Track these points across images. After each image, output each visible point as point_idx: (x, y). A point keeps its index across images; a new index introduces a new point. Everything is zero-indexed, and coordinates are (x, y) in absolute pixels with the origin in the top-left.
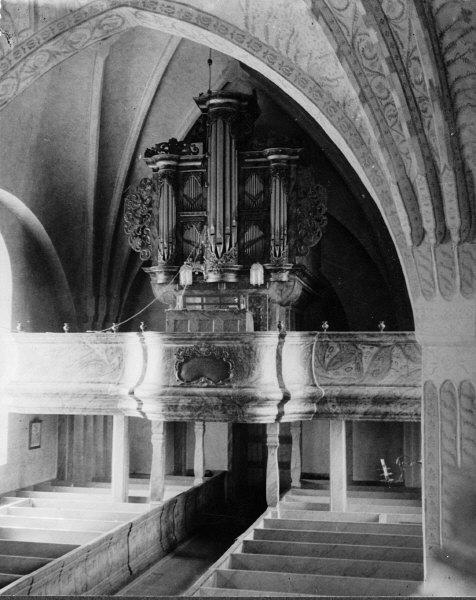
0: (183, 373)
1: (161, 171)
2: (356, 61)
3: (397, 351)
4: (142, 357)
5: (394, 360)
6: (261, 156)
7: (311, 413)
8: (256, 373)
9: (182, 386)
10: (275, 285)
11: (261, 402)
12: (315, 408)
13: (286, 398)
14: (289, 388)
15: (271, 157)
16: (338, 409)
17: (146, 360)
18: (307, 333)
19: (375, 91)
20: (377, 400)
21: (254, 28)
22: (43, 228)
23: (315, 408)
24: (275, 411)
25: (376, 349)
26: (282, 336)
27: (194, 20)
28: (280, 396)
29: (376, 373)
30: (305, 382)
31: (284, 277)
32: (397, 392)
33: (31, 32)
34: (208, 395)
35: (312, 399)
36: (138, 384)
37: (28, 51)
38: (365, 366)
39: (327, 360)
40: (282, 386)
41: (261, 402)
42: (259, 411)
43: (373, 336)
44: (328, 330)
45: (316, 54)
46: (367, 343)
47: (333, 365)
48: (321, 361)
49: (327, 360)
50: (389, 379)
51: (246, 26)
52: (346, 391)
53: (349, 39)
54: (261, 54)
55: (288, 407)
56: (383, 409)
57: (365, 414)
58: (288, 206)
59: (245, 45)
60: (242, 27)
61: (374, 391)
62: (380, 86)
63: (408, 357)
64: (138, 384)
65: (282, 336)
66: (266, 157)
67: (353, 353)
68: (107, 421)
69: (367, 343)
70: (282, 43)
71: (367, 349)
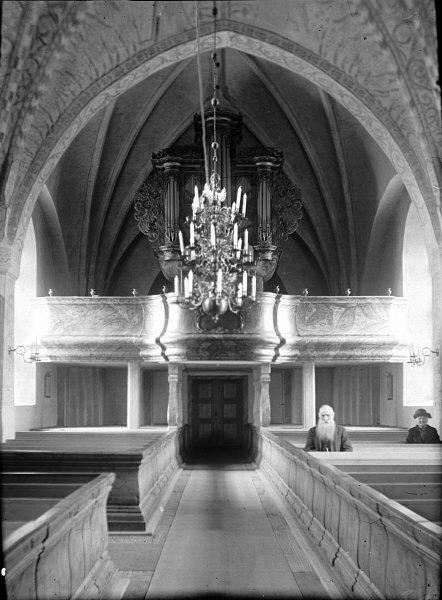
0: (203, 324)
1: (167, 170)
2: (410, 79)
3: (358, 310)
4: (163, 312)
5: (357, 317)
6: (251, 162)
7: (295, 356)
8: (261, 325)
9: (203, 333)
10: (261, 263)
11: (264, 344)
12: (297, 352)
13: (283, 342)
14: (283, 336)
15: (258, 164)
16: (315, 353)
17: (167, 316)
18: (293, 296)
19: (421, 99)
20: (345, 346)
21: (325, 54)
22: (56, 212)
23: (297, 352)
24: (273, 353)
25: (343, 309)
26: (278, 298)
27: (280, 44)
28: (278, 341)
29: (343, 327)
30: (292, 332)
31: (269, 256)
32: (361, 340)
33: (151, 43)
34: (225, 339)
35: (297, 346)
36: (162, 334)
37: (149, 56)
38: (335, 322)
39: (307, 318)
40: (279, 335)
41: (264, 344)
42: (263, 352)
43: (341, 299)
44: (309, 294)
45: (373, 74)
46: (337, 305)
47: (311, 322)
48: (301, 316)
49: (307, 318)
50: (352, 331)
51: (320, 51)
52: (323, 339)
53: (406, 64)
54: (330, 72)
55: (283, 351)
56: (348, 353)
57: (335, 357)
58: (271, 204)
59: (318, 65)
60: (317, 52)
61: (344, 340)
62: (425, 96)
63: (366, 315)
64: (162, 334)
65: (278, 298)
66: (254, 163)
67: (324, 314)
68: (122, 372)
69: (337, 305)
70: (347, 66)
71: (337, 309)
